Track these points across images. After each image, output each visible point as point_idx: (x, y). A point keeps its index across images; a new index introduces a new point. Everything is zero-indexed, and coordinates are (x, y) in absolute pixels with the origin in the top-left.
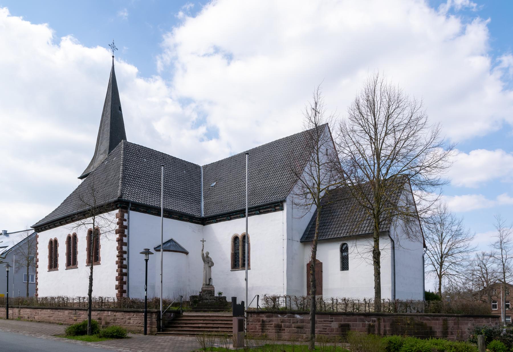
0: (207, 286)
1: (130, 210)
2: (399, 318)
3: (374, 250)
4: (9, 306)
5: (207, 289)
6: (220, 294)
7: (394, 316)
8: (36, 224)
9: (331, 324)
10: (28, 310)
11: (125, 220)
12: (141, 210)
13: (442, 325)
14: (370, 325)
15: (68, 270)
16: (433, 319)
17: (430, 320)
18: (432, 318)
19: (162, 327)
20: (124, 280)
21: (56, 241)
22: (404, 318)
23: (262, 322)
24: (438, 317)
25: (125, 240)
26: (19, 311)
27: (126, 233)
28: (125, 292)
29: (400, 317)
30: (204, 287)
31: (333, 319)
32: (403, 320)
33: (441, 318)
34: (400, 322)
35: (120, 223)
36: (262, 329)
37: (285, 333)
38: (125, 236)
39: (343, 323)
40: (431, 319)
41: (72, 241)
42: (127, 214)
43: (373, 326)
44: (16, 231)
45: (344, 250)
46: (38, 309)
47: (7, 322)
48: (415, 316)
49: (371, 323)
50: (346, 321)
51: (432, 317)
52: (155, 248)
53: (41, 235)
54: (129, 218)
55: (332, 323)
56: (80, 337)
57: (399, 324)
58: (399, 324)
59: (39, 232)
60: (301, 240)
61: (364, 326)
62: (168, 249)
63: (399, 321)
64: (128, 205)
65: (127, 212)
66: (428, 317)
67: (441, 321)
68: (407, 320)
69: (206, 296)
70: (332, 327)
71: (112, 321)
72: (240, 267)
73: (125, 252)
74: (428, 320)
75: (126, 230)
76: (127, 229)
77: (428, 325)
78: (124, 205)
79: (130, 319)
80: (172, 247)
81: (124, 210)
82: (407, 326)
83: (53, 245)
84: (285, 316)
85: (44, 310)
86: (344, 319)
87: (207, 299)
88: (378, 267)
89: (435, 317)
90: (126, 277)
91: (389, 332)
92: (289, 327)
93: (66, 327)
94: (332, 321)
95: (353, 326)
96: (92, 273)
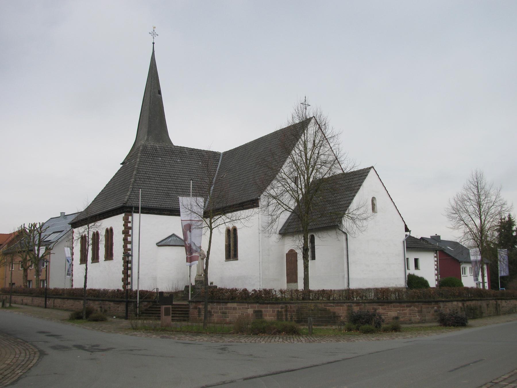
0: (199, 277)
1: (134, 213)
2: (304, 305)
3: (303, 247)
4: (47, 296)
5: (199, 279)
6: (212, 283)
7: (300, 304)
8: (73, 221)
9: (247, 310)
10: (59, 300)
11: (130, 222)
12: (144, 212)
13: (347, 310)
14: (278, 311)
15: (93, 264)
16: (337, 306)
17: (334, 307)
18: (335, 305)
19: (139, 313)
20: (129, 273)
21: (111, 229)
22: (309, 305)
23: (199, 309)
24: (342, 304)
25: (129, 239)
26: (54, 301)
27: (130, 233)
28: (128, 284)
29: (304, 304)
30: (196, 277)
31: (249, 306)
32: (307, 307)
33: (345, 305)
34: (305, 309)
35: (125, 225)
36: (199, 315)
37: (214, 317)
38: (130, 236)
39: (257, 309)
40: (335, 306)
41: (109, 233)
42: (131, 217)
43: (281, 312)
44: (73, 213)
45: (85, 286)
46: (65, 300)
47: (47, 310)
48: (318, 303)
49: (280, 310)
50: (260, 308)
51: (336, 304)
52: (157, 244)
53: (75, 230)
54: (132, 220)
55: (248, 309)
56: (79, 321)
57: (304, 310)
58: (304, 310)
59: (75, 228)
60: (279, 231)
61: (273, 311)
62: (169, 244)
63: (304, 308)
64: (132, 209)
65: (132, 215)
66: (331, 304)
67: (345, 307)
68: (311, 307)
69: (198, 286)
70: (248, 313)
71: (108, 309)
72: (231, 257)
73: (130, 250)
74: (331, 306)
75: (130, 231)
76: (131, 229)
77: (332, 310)
78: (129, 209)
79: (118, 307)
80: (172, 241)
81: (128, 214)
82: (311, 312)
83: (83, 239)
84: (214, 304)
85: (69, 300)
86: (257, 306)
87: (199, 289)
88: (306, 261)
89: (339, 304)
90: (130, 270)
91: (294, 317)
92: (216, 313)
93: (71, 313)
94: (249, 308)
95: (265, 312)
96: (86, 273)
